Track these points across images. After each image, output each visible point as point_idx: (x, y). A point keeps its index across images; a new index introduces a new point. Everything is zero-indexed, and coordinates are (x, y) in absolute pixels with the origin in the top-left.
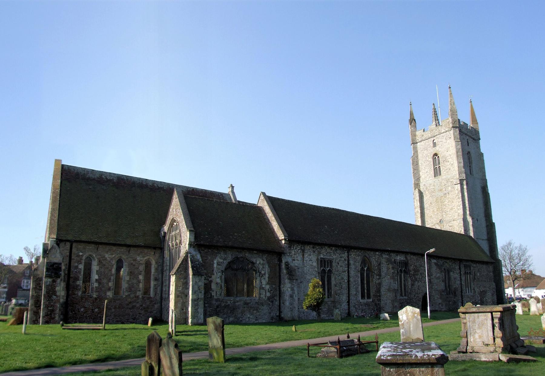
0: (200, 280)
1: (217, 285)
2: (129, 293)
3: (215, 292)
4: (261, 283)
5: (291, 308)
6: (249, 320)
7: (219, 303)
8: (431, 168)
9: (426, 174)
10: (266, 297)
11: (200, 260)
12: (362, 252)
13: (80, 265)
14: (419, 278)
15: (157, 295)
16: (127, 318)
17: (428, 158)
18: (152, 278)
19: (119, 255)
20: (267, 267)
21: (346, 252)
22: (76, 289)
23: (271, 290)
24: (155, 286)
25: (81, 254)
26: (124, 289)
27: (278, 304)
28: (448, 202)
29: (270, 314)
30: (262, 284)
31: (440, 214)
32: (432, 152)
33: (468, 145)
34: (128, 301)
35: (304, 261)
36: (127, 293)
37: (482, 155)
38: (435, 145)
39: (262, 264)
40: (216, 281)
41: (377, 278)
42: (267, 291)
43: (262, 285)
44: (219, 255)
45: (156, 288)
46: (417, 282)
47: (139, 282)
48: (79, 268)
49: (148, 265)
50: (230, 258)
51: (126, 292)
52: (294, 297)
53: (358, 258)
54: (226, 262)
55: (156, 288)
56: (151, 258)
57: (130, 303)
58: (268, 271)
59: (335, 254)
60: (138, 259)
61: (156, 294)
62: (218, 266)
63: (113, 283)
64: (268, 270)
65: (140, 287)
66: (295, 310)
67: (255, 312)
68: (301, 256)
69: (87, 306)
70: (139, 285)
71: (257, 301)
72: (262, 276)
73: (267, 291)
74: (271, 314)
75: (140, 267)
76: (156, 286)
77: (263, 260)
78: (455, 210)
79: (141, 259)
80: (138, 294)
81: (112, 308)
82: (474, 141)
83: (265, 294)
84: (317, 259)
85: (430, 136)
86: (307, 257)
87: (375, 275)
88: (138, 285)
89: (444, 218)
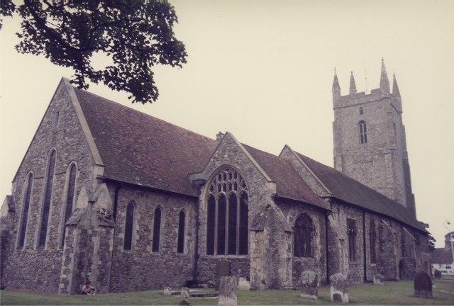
38: (361, 112)
49: (182, 215)
50: (297, 213)
54: (295, 218)
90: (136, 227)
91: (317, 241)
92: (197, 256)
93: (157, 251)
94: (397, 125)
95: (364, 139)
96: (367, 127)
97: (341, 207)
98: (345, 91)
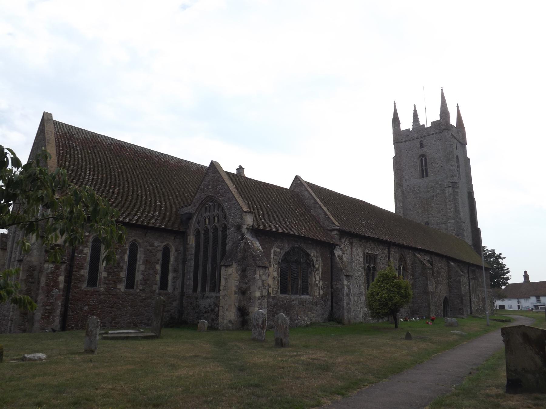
0: (264, 273)
1: (274, 279)
2: (144, 287)
3: (272, 288)
4: (315, 278)
5: (347, 309)
6: (304, 322)
7: (276, 301)
8: (417, 170)
9: (410, 175)
10: (319, 295)
11: (261, 248)
12: (399, 249)
13: (86, 249)
14: (441, 281)
15: (176, 290)
16: (140, 319)
17: (413, 159)
18: (171, 268)
19: (134, 238)
20: (320, 260)
21: (387, 248)
22: (79, 281)
23: (324, 288)
24: (174, 279)
25: (87, 234)
26: (138, 281)
27: (331, 304)
28: (436, 205)
29: (323, 316)
30: (316, 280)
31: (425, 216)
32: (418, 153)
33: (457, 149)
34: (142, 297)
35: (353, 256)
36: (142, 287)
37: (467, 160)
38: (422, 146)
39: (316, 256)
40: (273, 275)
41: (410, 278)
42: (320, 288)
43: (316, 282)
44: (276, 244)
45: (175, 282)
46: (439, 285)
47: (156, 273)
48: (84, 253)
49: (166, 252)
50: (287, 248)
51: (141, 285)
52: (350, 296)
53: (396, 255)
54: (283, 253)
55: (175, 282)
56: (171, 244)
57: (145, 299)
58: (321, 266)
59: (378, 249)
60: (155, 244)
61: (174, 289)
62: (275, 257)
63: (125, 273)
64: (321, 264)
65: (157, 280)
66: (350, 312)
67: (310, 313)
68: (350, 250)
69: (92, 303)
70: (155, 277)
71: (311, 300)
72: (316, 271)
73: (320, 288)
74: (324, 316)
75: (157, 255)
76: (175, 278)
77: (317, 253)
78: (443, 212)
79: (159, 244)
80: (154, 288)
81: (128, 305)
82: (461, 145)
83: (318, 291)
84: (364, 254)
85: (416, 136)
86: (355, 251)
87: (409, 275)
88: (155, 276)
89: (430, 220)
90: (140, 266)
91: (317, 278)
92: (182, 294)
93: (132, 287)
94: (460, 157)
95: (424, 173)
96: (428, 161)
97: (355, 241)
98: (406, 124)
